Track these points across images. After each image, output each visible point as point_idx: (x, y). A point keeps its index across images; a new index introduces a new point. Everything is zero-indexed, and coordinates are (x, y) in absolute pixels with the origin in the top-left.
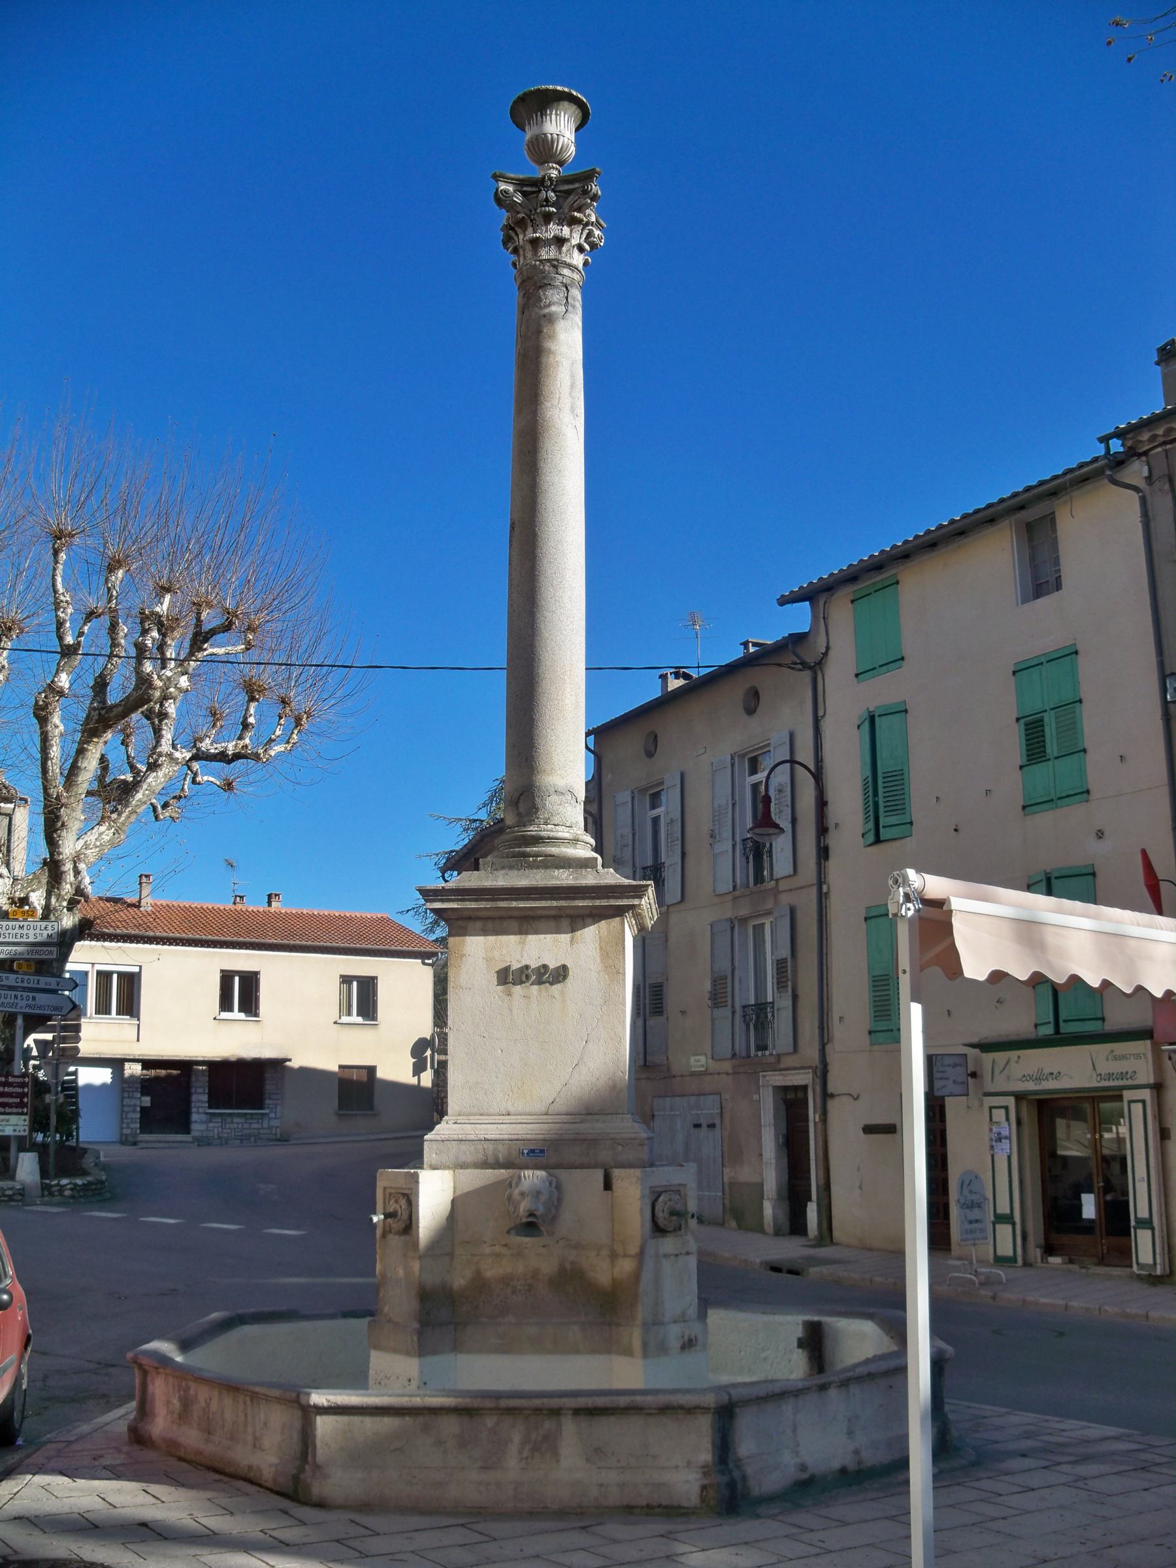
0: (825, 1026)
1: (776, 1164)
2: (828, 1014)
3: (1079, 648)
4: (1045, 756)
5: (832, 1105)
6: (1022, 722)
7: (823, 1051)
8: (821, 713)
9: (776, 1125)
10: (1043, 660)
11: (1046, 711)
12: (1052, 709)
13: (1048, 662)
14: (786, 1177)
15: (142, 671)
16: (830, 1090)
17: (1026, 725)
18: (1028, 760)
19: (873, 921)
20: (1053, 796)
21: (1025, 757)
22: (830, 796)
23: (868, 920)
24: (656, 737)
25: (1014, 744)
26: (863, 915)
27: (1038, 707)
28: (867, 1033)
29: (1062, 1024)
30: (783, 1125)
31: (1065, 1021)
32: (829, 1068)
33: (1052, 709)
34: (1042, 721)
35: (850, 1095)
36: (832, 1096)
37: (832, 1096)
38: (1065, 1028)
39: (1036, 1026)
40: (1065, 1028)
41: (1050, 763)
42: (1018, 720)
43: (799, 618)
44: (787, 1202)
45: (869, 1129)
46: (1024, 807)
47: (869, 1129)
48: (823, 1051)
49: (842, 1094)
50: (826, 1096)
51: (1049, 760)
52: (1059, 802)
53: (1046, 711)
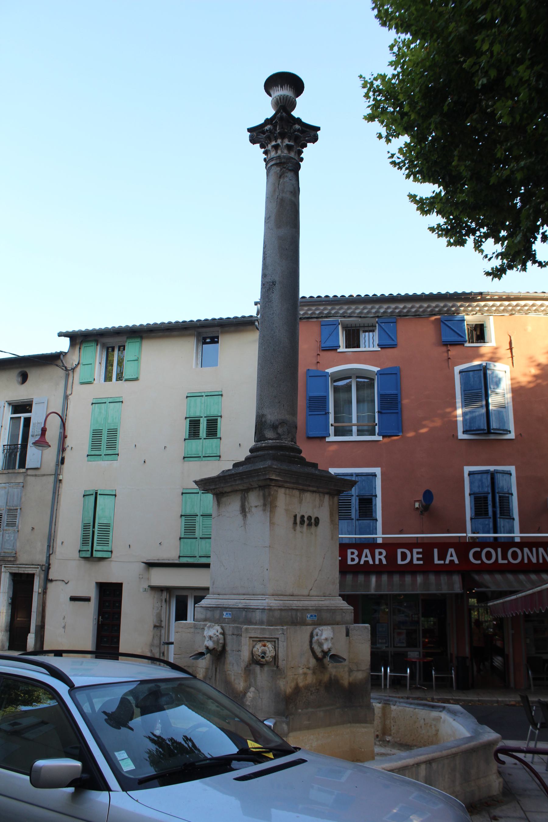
0: (52, 544)
1: (6, 612)
2: (54, 540)
3: (224, 393)
4: (199, 437)
5: (50, 586)
6: (188, 419)
7: (49, 557)
8: (69, 392)
9: (8, 592)
10: (203, 394)
11: (202, 417)
12: (205, 417)
13: (206, 396)
14: (9, 620)
15: (493, 234)
16: (50, 577)
17: (190, 421)
18: (189, 437)
19: (87, 497)
20: (200, 455)
21: (188, 433)
22: (68, 433)
23: (85, 497)
24: (90, 383)
25: (184, 428)
26: (83, 494)
27: (198, 414)
28: (78, 551)
29: (94, 552)
30: (11, 593)
31: (96, 551)
32: (51, 566)
33: (205, 417)
34: (200, 421)
35: (63, 581)
36: (51, 581)
37: (51, 581)
38: (95, 554)
39: (180, 557)
40: (95, 554)
41: (201, 440)
42: (186, 418)
43: (64, 345)
44: (9, 633)
45: (73, 599)
46: (184, 458)
47: (73, 599)
48: (49, 557)
49: (58, 580)
50: (47, 580)
51: (201, 439)
52: (204, 459)
53: (202, 417)
